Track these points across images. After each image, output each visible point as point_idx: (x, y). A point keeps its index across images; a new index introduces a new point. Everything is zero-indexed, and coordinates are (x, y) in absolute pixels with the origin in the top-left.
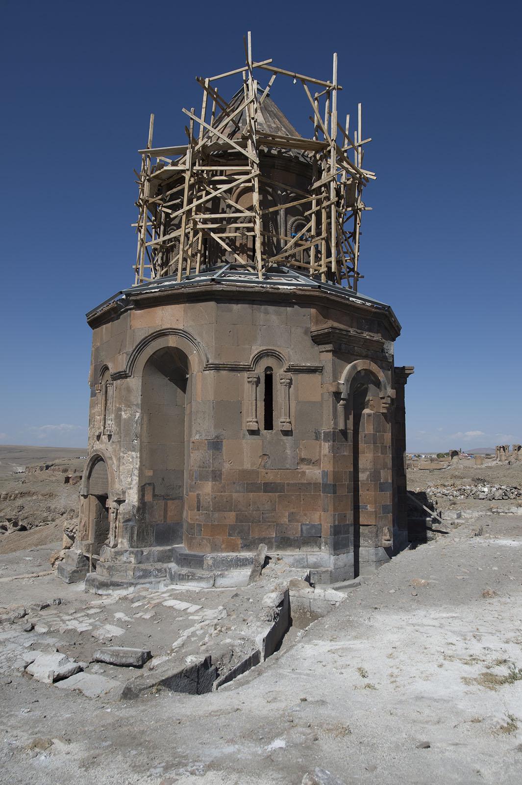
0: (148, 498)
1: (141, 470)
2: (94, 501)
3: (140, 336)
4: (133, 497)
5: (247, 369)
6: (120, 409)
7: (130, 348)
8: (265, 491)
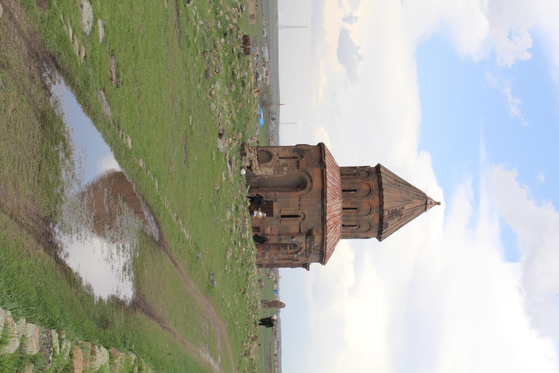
0: (258, 178)
1: (267, 175)
3: (311, 174)
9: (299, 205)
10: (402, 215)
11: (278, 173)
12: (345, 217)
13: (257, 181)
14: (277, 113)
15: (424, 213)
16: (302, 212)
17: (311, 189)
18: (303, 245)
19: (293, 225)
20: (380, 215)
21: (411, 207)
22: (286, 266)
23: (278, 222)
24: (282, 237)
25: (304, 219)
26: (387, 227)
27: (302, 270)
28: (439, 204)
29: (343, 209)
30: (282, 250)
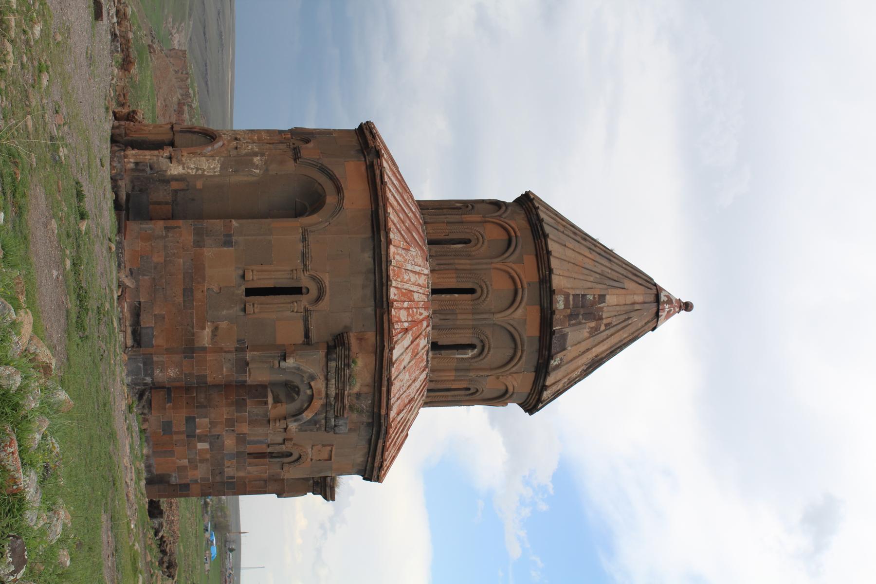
0: (175, 185)
1: (202, 176)
2: (167, 137)
3: (337, 172)
4: (175, 170)
5: (305, 268)
6: (262, 155)
7: (326, 162)
8: (184, 290)
9: (304, 256)
10: (601, 318)
11: (236, 171)
12: (441, 318)
13: (169, 198)
14: (238, 542)
15: (649, 337)
16: (313, 278)
17: (339, 206)
18: (319, 385)
19: (283, 319)
20: (542, 310)
21: (622, 302)
22: (260, 488)
23: (236, 310)
24: (249, 355)
25: (319, 299)
26: (564, 349)
27: (313, 500)
28: (687, 307)
29: (435, 291)
30: (252, 408)
